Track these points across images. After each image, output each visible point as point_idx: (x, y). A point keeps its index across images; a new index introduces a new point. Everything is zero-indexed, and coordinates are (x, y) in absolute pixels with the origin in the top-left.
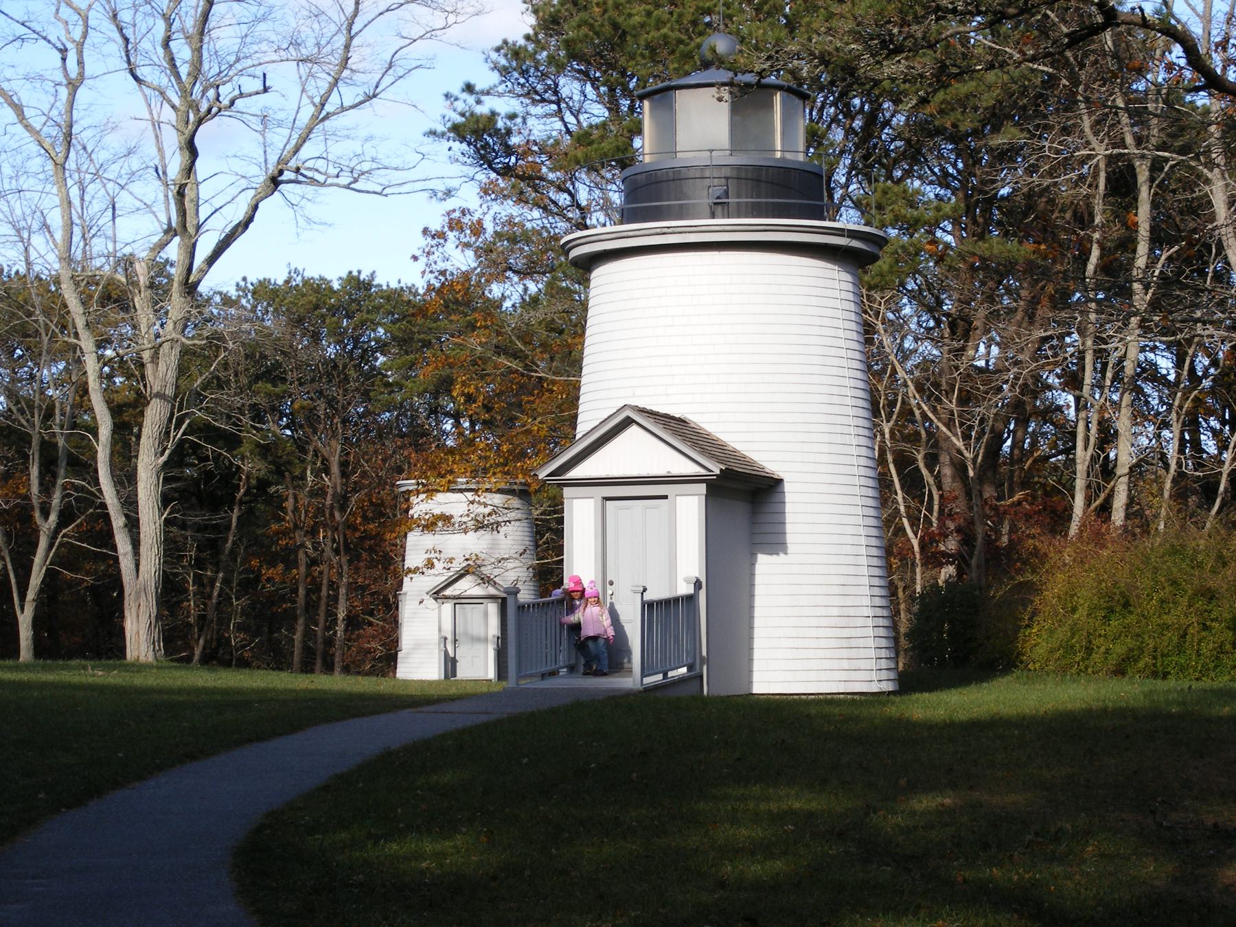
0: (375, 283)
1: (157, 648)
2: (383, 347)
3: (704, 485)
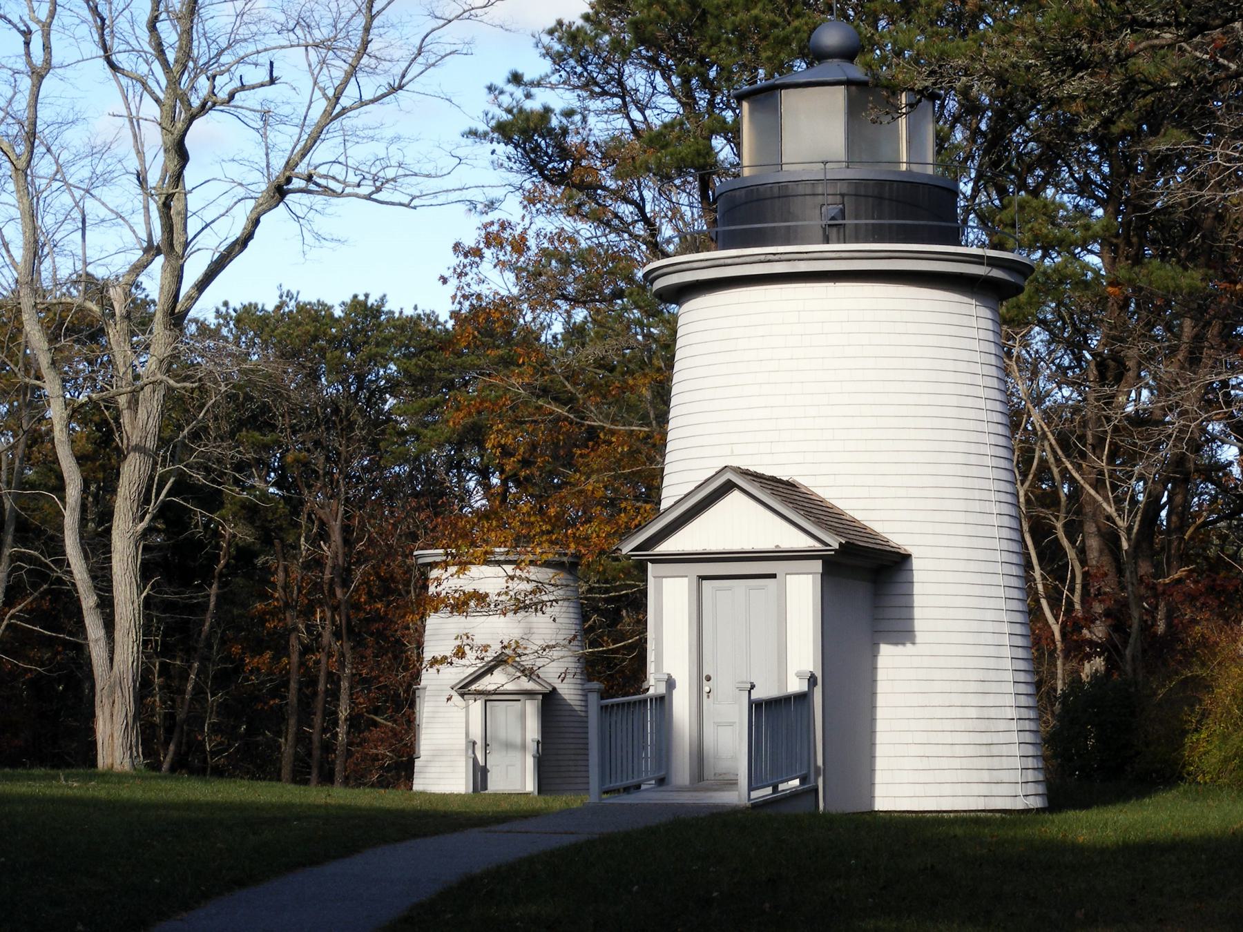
0: (385, 309)
1: (135, 754)
2: (393, 387)
3: (820, 562)
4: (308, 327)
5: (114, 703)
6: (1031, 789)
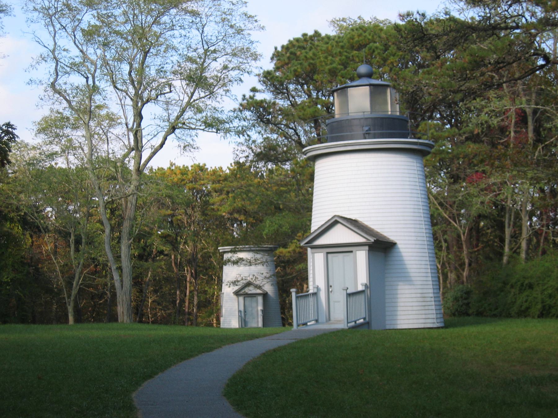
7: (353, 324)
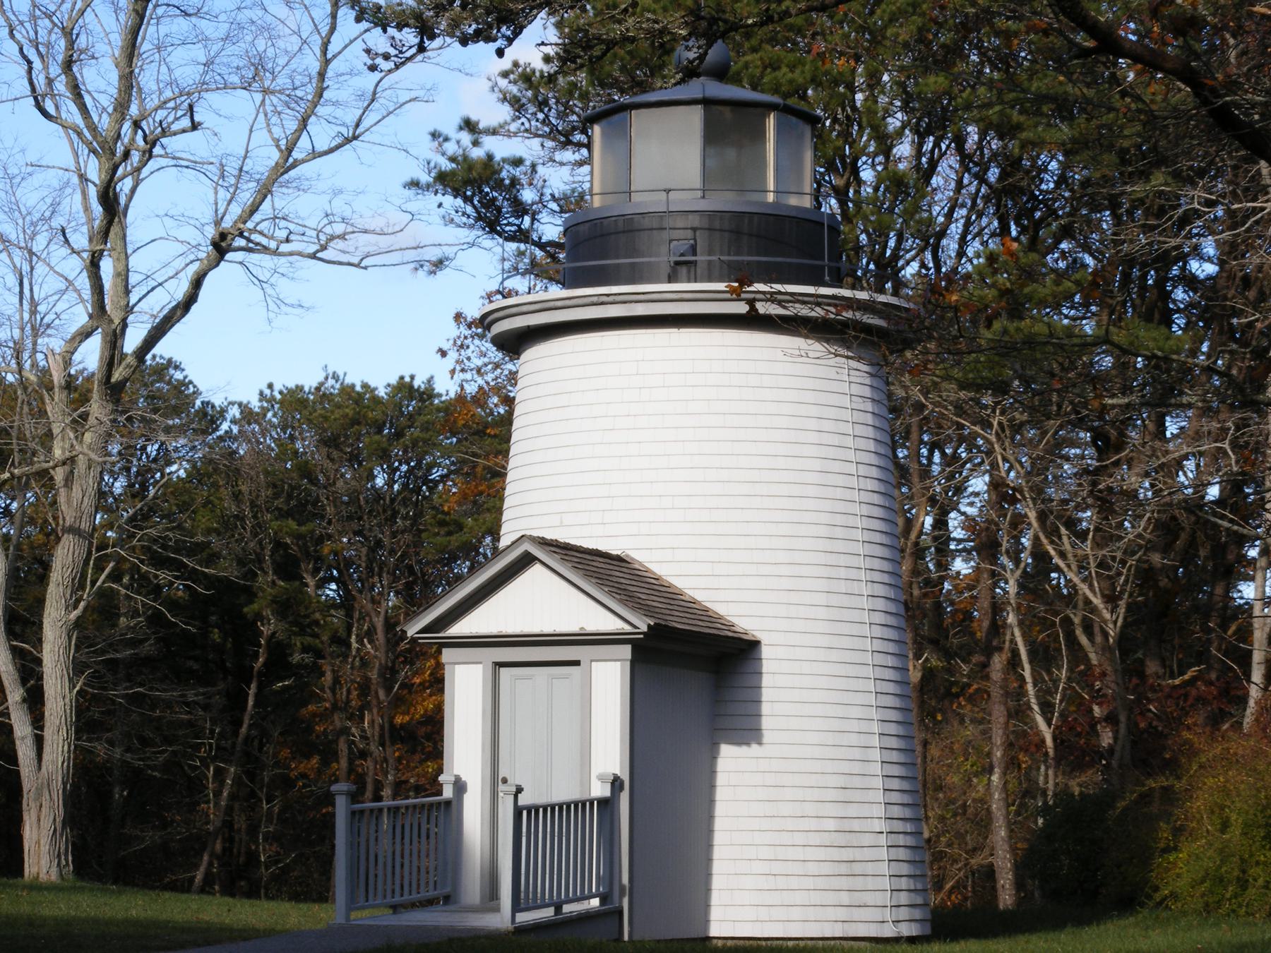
1: (64, 862)
4: (347, 410)
5: (41, 806)
6: (904, 913)
7: (548, 913)
